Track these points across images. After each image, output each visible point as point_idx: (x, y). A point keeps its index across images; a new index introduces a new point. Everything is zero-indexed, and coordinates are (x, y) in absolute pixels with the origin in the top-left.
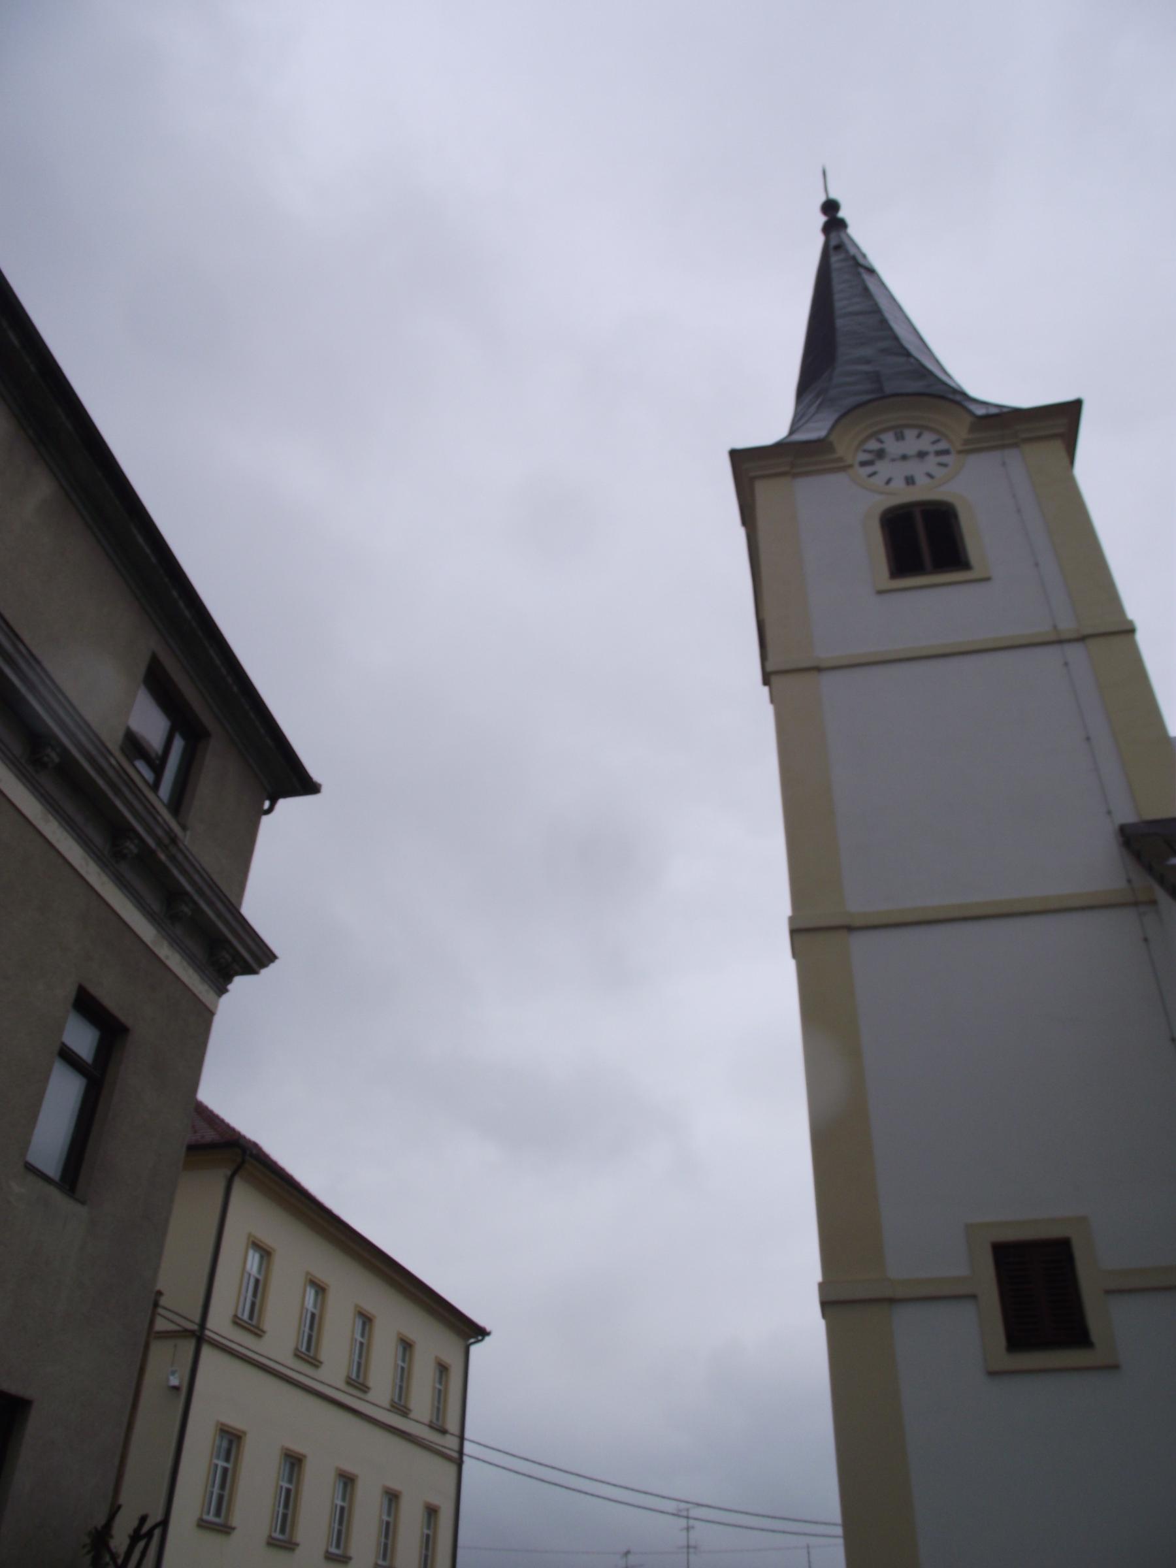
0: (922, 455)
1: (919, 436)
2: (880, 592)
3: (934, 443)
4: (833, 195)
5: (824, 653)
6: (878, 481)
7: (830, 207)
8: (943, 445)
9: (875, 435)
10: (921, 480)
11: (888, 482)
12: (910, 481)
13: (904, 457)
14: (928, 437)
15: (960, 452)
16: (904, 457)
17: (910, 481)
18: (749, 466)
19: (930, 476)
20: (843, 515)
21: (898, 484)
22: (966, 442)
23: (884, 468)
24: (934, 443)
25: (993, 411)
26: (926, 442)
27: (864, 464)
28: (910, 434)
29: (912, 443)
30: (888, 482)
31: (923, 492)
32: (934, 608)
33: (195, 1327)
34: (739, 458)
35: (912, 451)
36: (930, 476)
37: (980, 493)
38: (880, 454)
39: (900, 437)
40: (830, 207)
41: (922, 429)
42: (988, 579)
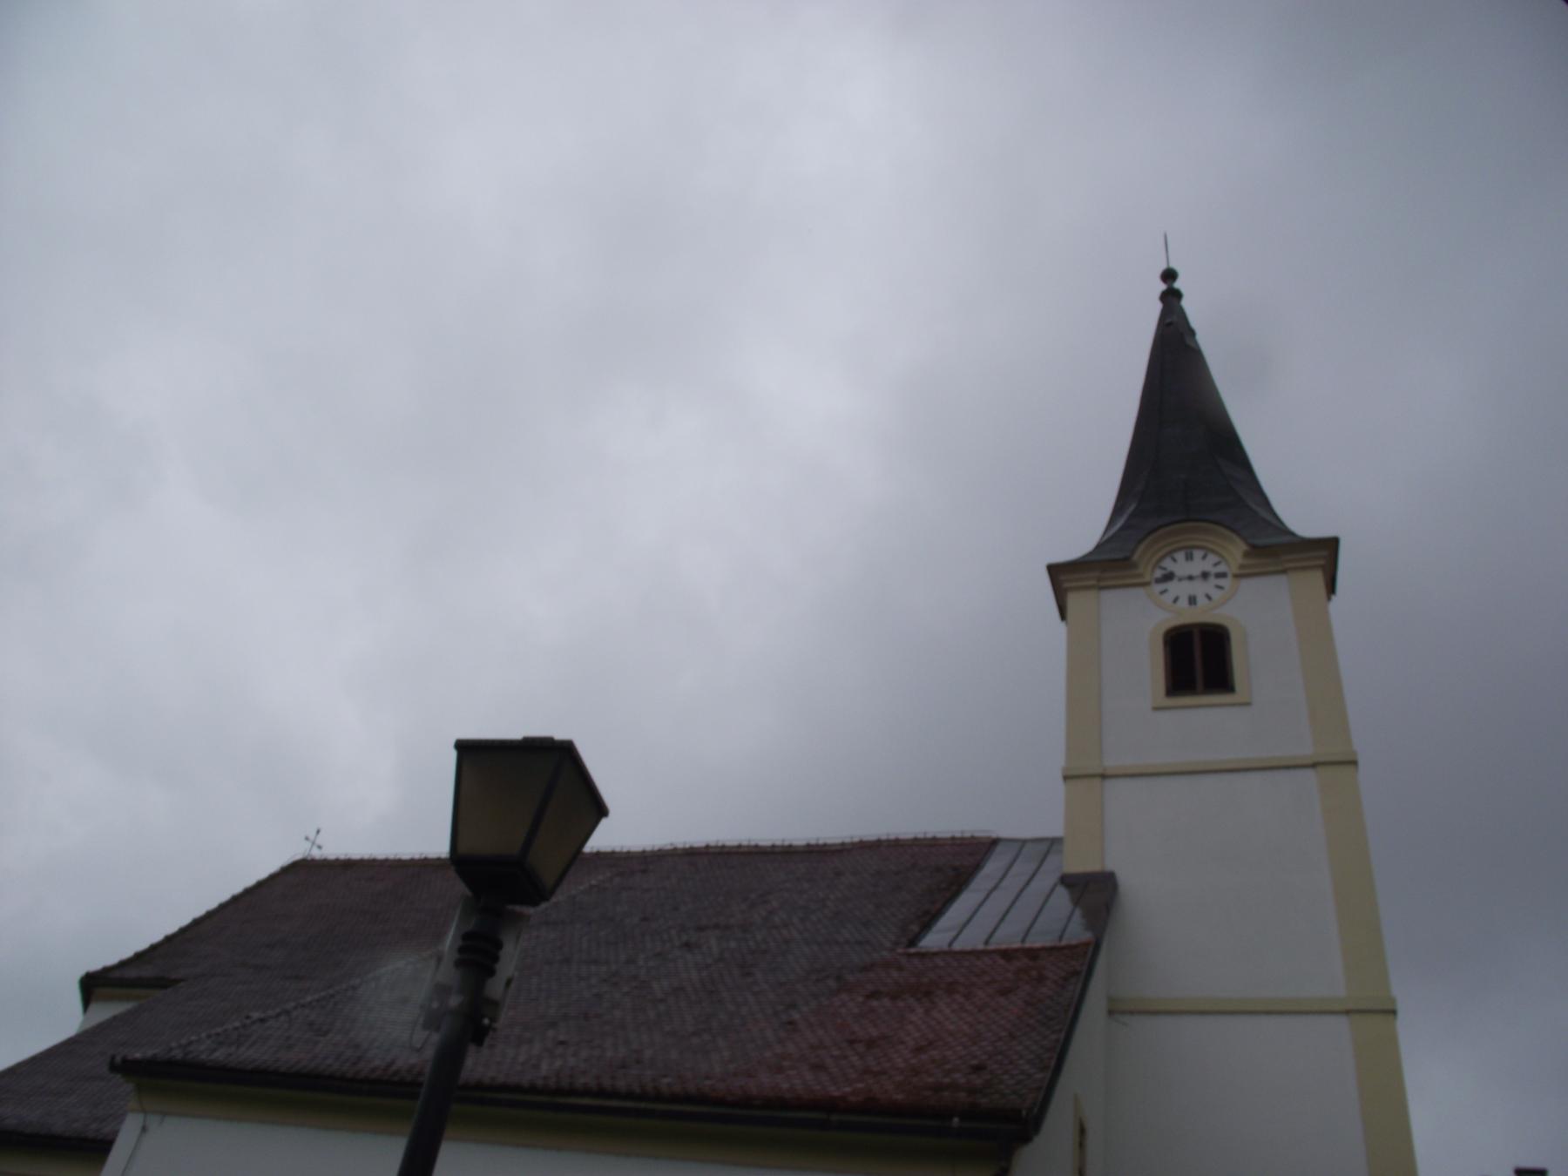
0: (1205, 575)
1: (1204, 557)
2: (1156, 709)
3: (1216, 565)
4: (1173, 265)
5: (1111, 762)
6: (1168, 598)
7: (1169, 275)
8: (1222, 568)
9: (1157, 565)
10: (1201, 601)
11: (1176, 600)
12: (1192, 600)
13: (1191, 578)
14: (1212, 558)
15: (1236, 576)
16: (1191, 578)
17: (1192, 600)
18: (1062, 576)
19: (1209, 597)
20: (1137, 621)
21: (1183, 602)
22: (1242, 567)
23: (1173, 588)
24: (1216, 565)
25: (1274, 522)
26: (1208, 565)
27: (1158, 581)
28: (1198, 554)
29: (1198, 565)
30: (1176, 600)
31: (1201, 614)
32: (1205, 724)
33: (1063, 578)
34: (1055, 571)
35: (1196, 571)
36: (1209, 597)
37: (1256, 612)
38: (1169, 577)
39: (1189, 557)
40: (1169, 275)
41: (1207, 551)
42: (1248, 704)
